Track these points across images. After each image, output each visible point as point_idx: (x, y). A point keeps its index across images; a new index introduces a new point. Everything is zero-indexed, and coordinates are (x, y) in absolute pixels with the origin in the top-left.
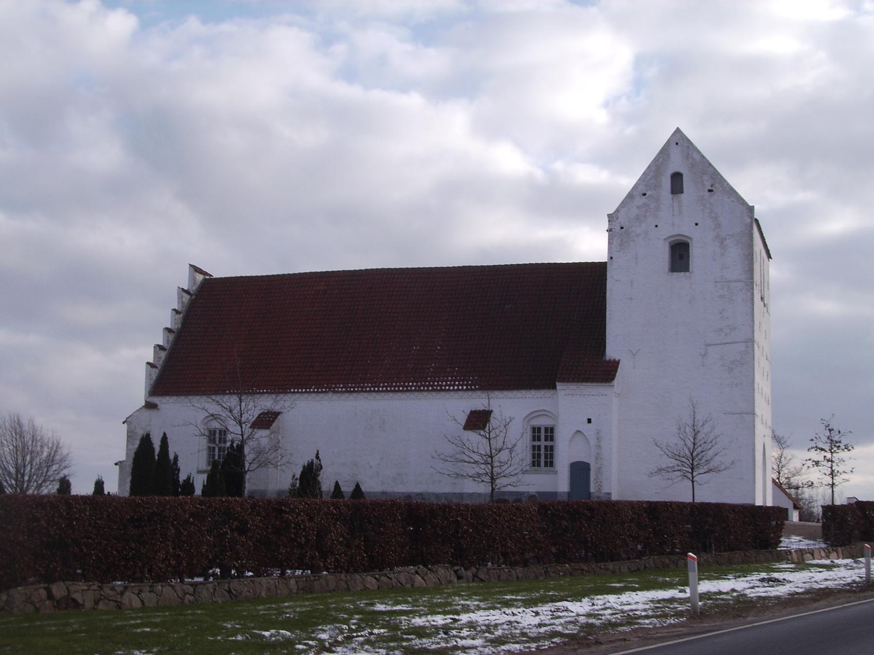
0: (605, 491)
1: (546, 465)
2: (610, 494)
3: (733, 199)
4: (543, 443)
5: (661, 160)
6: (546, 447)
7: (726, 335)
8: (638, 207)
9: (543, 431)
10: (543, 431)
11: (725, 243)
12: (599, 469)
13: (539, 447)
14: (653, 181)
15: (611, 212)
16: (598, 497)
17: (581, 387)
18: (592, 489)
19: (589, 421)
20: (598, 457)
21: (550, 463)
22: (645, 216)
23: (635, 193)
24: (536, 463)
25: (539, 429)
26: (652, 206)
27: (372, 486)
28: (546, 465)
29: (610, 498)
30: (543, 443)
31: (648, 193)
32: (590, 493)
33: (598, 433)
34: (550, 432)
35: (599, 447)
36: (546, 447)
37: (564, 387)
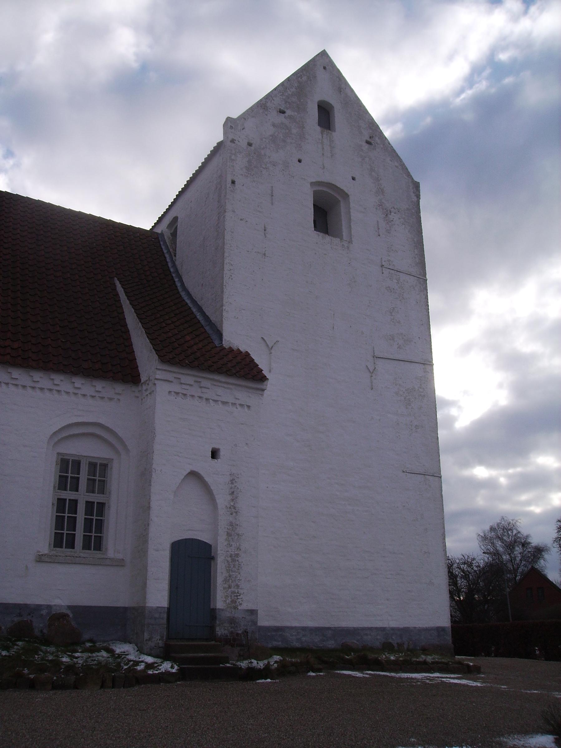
0: (245, 606)
1: (87, 546)
2: (253, 612)
3: (396, 164)
4: (82, 496)
5: (304, 78)
6: (89, 505)
7: (399, 347)
8: (274, 125)
9: (84, 469)
10: (84, 469)
11: (391, 217)
12: (234, 558)
13: (74, 503)
14: (294, 99)
15: (235, 115)
16: (232, 621)
17: (205, 383)
18: (220, 601)
19: (214, 454)
20: (233, 532)
21: (94, 543)
22: (284, 141)
23: (269, 104)
24: (62, 539)
25: (77, 464)
26: (294, 131)
27: (139, 368)
28: (87, 546)
29: (255, 623)
30: (82, 496)
31: (289, 112)
32: (213, 614)
33: (232, 481)
34: (99, 471)
35: (233, 510)
36: (89, 505)
37: (169, 376)
